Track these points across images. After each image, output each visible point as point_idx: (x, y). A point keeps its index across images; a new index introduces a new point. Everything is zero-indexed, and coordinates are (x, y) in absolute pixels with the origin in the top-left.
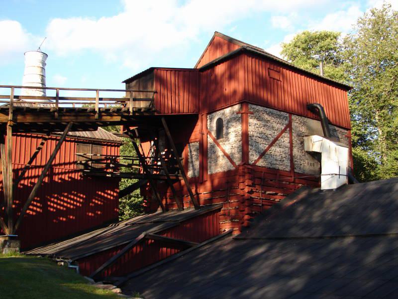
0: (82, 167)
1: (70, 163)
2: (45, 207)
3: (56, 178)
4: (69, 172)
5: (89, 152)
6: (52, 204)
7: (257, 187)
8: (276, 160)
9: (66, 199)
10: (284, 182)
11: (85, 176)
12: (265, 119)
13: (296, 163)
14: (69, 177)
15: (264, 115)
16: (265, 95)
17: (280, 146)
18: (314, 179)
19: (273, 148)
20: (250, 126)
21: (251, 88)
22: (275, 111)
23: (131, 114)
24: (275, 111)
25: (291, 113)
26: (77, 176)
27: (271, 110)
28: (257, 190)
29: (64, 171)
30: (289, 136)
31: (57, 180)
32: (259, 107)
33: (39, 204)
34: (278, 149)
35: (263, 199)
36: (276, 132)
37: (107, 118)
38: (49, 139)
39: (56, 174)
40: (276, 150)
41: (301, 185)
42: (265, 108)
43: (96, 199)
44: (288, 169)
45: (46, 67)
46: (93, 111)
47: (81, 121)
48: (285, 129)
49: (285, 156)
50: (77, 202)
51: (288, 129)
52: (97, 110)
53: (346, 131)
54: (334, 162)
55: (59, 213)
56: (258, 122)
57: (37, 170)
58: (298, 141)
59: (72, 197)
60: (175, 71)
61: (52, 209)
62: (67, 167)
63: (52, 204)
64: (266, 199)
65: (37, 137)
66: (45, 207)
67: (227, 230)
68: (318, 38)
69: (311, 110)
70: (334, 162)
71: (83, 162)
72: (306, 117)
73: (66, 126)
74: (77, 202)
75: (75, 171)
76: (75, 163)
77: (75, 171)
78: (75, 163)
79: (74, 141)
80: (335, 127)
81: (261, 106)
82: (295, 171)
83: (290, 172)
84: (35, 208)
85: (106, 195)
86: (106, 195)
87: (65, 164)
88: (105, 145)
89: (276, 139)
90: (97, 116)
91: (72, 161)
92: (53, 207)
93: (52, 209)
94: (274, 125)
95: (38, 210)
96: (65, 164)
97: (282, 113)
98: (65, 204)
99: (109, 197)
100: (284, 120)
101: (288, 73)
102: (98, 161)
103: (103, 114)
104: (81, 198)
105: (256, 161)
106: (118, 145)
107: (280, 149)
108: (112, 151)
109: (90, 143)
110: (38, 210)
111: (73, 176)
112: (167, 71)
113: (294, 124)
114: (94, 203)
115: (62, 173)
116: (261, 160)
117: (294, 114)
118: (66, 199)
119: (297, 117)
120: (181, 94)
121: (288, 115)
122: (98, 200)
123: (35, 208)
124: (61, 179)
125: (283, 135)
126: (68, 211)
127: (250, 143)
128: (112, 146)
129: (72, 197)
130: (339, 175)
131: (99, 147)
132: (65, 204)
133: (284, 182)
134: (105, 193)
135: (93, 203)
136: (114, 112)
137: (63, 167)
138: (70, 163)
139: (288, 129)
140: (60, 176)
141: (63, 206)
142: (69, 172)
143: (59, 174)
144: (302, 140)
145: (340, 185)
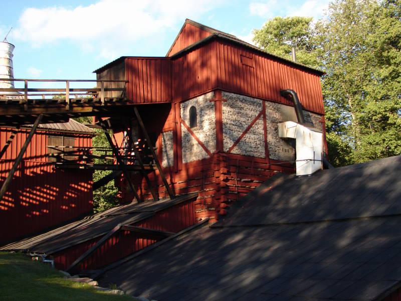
0: (54, 160)
1: (41, 156)
2: (17, 201)
3: (28, 172)
4: (41, 166)
5: (61, 144)
6: (24, 199)
7: (232, 174)
8: (251, 147)
9: (38, 193)
10: (259, 169)
11: (58, 169)
12: (239, 106)
13: (270, 149)
14: (41, 171)
15: (238, 102)
16: (239, 82)
17: (254, 133)
18: (290, 166)
19: (247, 135)
20: (223, 113)
21: (223, 76)
22: (248, 98)
23: (103, 105)
24: (248, 97)
25: (265, 99)
26: (49, 169)
27: (245, 97)
28: (232, 177)
29: (35, 164)
30: (263, 122)
31: (28, 174)
32: (232, 94)
33: (10, 199)
34: (253, 136)
35: (238, 187)
36: (250, 119)
37: (78, 109)
38: (19, 132)
39: (27, 168)
40: (250, 138)
41: (276, 171)
42: (238, 95)
43: (69, 192)
44: (263, 156)
45: (13, 59)
46: (64, 102)
47: (52, 112)
48: (259, 116)
49: (259, 143)
50: (50, 195)
51: (262, 116)
52: (67, 101)
53: (319, 117)
54: (309, 148)
55: (32, 207)
56: (232, 110)
57: (8, 164)
58: (272, 128)
59: (45, 190)
60: (147, 59)
61: (24, 204)
62: (39, 160)
63: (24, 199)
64: (241, 187)
65: (7, 131)
66: (17, 201)
67: (203, 219)
68: (290, 24)
69: (284, 97)
70: (309, 148)
71: (55, 155)
72: (279, 103)
73: (36, 118)
74: (50, 195)
75: (48, 164)
76: (47, 155)
77: (48, 164)
78: (47, 155)
79: (45, 134)
80: (309, 113)
81: (235, 93)
82: (270, 157)
83: (265, 159)
84: (7, 203)
85: (79, 188)
86: (79, 188)
87: (36, 157)
88: (77, 137)
89: (250, 127)
90: (67, 107)
91: (44, 153)
92: (25, 201)
93: (24, 204)
94: (248, 112)
95: (10, 204)
96: (36, 157)
97: (255, 100)
98: (38, 198)
99: (83, 189)
100: (258, 107)
101: (261, 59)
102: (71, 153)
103: (74, 105)
104: (54, 191)
105: (231, 149)
106: (90, 136)
107: (254, 136)
108: (85, 143)
109: (61, 135)
110: (10, 204)
111: (46, 170)
112: (138, 59)
113: (269, 111)
114: (68, 196)
115: (33, 167)
116: (236, 148)
117: (268, 101)
118: (38, 193)
119: (271, 103)
120: (153, 83)
121: (261, 102)
122: (72, 193)
123: (7, 203)
124: (33, 172)
125: (257, 121)
126: (42, 205)
127: (224, 131)
128: (84, 137)
129: (45, 190)
130: (314, 160)
131: (71, 139)
132: (38, 198)
133: (259, 169)
134: (78, 185)
135: (66, 195)
136: (85, 103)
137: (34, 160)
138: (41, 156)
139: (262, 116)
140: (32, 170)
141: (35, 200)
142: (41, 166)
143: (30, 167)
144: (276, 126)
145: (314, 172)
